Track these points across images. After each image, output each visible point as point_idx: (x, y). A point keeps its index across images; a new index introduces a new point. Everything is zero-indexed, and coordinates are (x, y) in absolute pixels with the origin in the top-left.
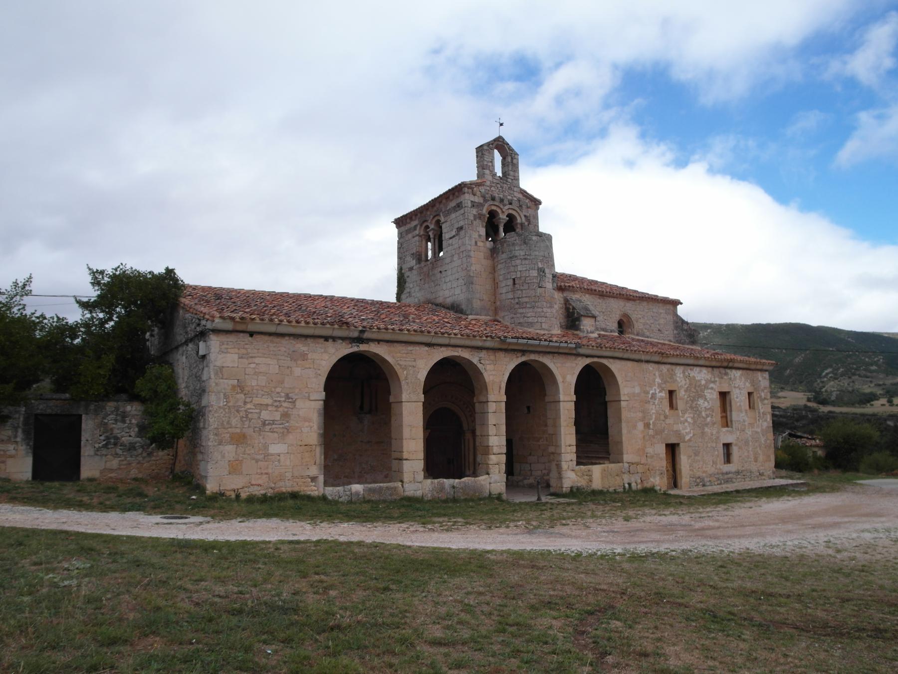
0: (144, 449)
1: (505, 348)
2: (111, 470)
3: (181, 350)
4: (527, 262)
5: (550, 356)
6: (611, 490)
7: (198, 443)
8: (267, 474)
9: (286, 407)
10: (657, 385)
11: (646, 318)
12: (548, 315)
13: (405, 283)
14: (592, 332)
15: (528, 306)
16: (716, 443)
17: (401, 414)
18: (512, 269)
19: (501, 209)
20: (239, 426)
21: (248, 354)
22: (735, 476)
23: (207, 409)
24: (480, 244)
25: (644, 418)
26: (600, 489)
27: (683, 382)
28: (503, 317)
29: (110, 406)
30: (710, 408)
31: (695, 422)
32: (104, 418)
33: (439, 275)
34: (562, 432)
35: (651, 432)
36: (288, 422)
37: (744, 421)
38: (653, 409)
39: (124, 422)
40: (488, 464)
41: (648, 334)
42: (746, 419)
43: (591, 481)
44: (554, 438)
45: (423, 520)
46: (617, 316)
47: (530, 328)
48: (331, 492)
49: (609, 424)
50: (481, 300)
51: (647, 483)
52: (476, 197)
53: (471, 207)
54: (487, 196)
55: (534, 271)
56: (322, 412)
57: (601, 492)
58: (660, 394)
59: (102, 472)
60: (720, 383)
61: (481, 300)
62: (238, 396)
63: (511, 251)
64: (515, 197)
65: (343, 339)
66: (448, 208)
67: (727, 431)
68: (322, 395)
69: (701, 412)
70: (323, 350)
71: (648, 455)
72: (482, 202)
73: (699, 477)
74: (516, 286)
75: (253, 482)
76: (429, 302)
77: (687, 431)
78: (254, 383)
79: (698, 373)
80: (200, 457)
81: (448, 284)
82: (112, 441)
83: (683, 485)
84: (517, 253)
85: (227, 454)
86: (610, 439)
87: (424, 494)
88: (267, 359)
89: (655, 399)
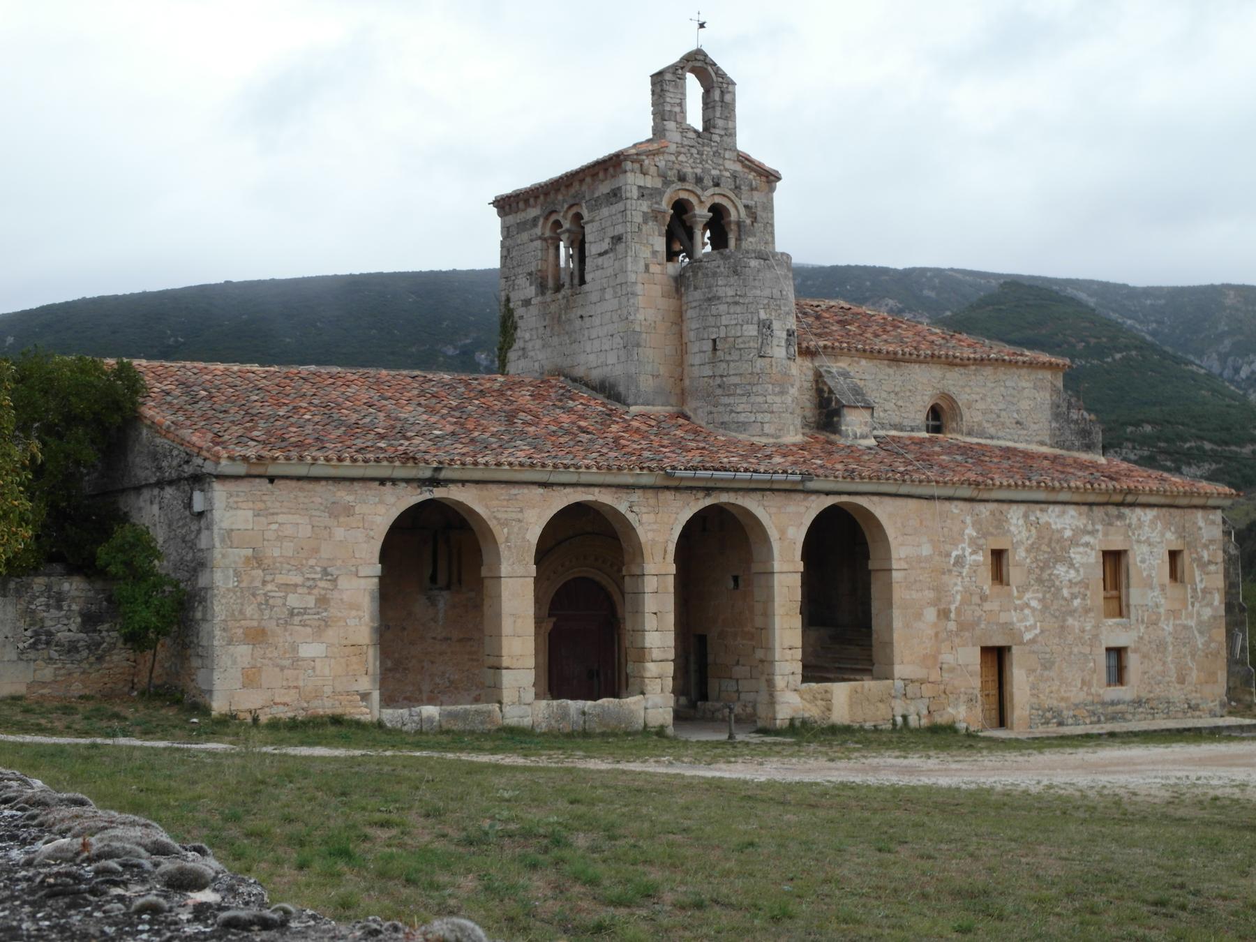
0: (90, 650)
1: (674, 486)
2: (44, 684)
3: (146, 494)
4: (738, 309)
5: (758, 495)
6: (868, 725)
7: (191, 642)
8: (296, 687)
9: (323, 589)
10: (967, 541)
11: (989, 400)
12: (775, 408)
13: (516, 328)
14: (864, 437)
15: (738, 391)
16: (1091, 646)
17: (500, 596)
18: (711, 321)
19: (699, 197)
20: (255, 617)
21: (266, 509)
22: (1131, 709)
23: (210, 592)
24: (655, 269)
25: (935, 603)
26: (847, 722)
27: (1025, 534)
28: (695, 409)
29: (39, 582)
30: (1080, 582)
31: (1046, 608)
32: (30, 603)
33: (578, 322)
34: (777, 625)
35: (952, 626)
36: (326, 610)
37: (1157, 606)
38: (956, 586)
39: (60, 608)
40: (643, 678)
41: (992, 431)
42: (1163, 601)
43: (829, 710)
44: (761, 636)
45: (525, 752)
46: (926, 398)
47: (741, 432)
48: (391, 716)
49: (874, 611)
50: (655, 376)
51: (941, 716)
52: (649, 178)
53: (638, 199)
54: (669, 173)
55: (751, 327)
56: (377, 595)
57: (847, 730)
58: (974, 557)
59: (29, 686)
60: (1106, 534)
61: (655, 376)
62: (254, 572)
63: (710, 287)
64: (726, 170)
65: (408, 481)
66: (596, 195)
67: (1118, 624)
68: (377, 569)
69: (1059, 589)
70: (377, 499)
71: (945, 666)
72: (660, 186)
73: (1051, 709)
74: (718, 353)
75: (277, 700)
76: (559, 372)
77: (1028, 624)
78: (276, 553)
79: (1058, 516)
80: (195, 662)
81: (595, 342)
82: (44, 638)
83: (1016, 721)
84: (721, 292)
85: (239, 659)
86: (874, 636)
87: (536, 724)
88: (295, 516)
89: (963, 567)
